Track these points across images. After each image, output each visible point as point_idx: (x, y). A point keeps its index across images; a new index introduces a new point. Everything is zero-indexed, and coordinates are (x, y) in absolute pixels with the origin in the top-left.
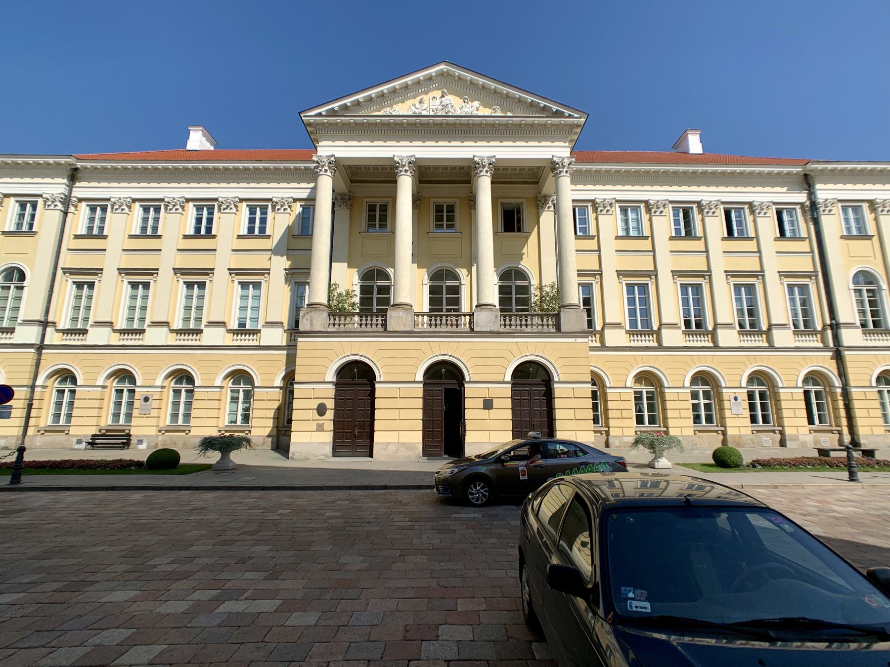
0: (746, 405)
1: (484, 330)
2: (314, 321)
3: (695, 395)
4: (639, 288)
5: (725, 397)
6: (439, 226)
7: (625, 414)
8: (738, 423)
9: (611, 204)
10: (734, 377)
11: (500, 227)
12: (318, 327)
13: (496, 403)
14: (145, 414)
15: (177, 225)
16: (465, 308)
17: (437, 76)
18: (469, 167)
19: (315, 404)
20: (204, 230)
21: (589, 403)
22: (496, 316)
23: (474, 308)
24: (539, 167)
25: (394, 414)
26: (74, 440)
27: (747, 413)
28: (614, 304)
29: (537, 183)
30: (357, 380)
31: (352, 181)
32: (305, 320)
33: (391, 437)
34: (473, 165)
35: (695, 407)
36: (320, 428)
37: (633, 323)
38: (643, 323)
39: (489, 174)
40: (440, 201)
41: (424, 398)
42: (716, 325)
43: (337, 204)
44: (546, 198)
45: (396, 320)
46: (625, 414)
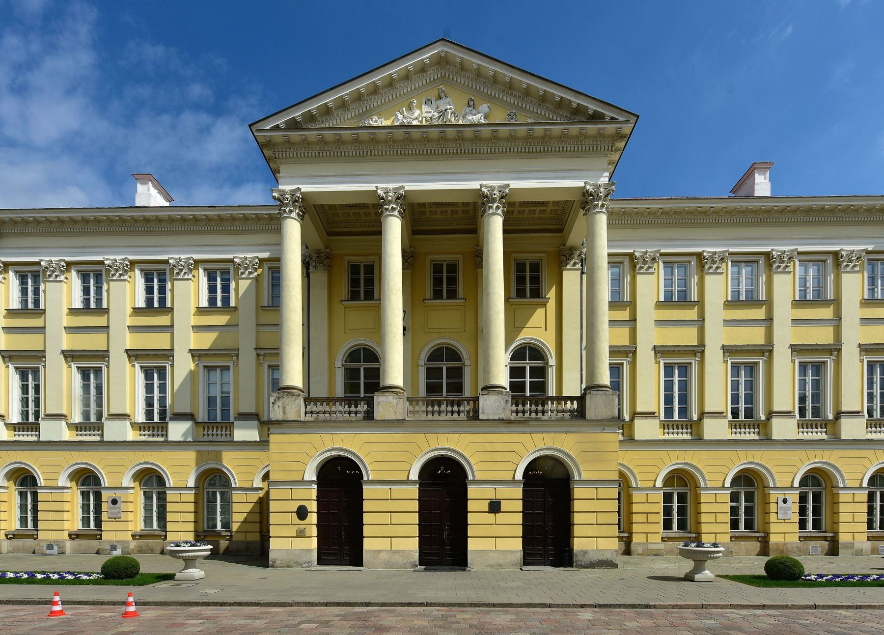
0: (796, 508)
1: (491, 417)
2: (288, 408)
3: (735, 497)
4: (680, 365)
5: (773, 499)
6: (437, 295)
7: (652, 518)
8: (784, 530)
9: (654, 259)
10: (785, 472)
11: (513, 293)
12: (292, 416)
13: (504, 506)
14: (116, 519)
15: (128, 293)
16: (467, 392)
17: (432, 65)
18: (475, 204)
19: (294, 506)
20: (157, 304)
21: (614, 506)
22: (507, 401)
23: (479, 391)
24: (566, 203)
25: (385, 519)
26: (44, 545)
27: (796, 518)
28: (649, 388)
29: (561, 231)
30: (341, 483)
31: (329, 234)
32: (276, 406)
33: (382, 544)
34: (480, 201)
35: (734, 511)
36: (301, 534)
37: (669, 412)
38: (681, 412)
39: (500, 211)
40: (438, 258)
41: (420, 500)
42: (838, 415)
43: (312, 264)
44: (572, 249)
45: (386, 406)
46: (652, 518)
